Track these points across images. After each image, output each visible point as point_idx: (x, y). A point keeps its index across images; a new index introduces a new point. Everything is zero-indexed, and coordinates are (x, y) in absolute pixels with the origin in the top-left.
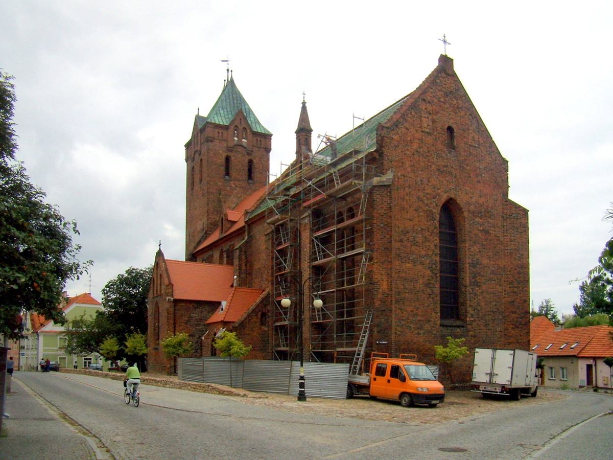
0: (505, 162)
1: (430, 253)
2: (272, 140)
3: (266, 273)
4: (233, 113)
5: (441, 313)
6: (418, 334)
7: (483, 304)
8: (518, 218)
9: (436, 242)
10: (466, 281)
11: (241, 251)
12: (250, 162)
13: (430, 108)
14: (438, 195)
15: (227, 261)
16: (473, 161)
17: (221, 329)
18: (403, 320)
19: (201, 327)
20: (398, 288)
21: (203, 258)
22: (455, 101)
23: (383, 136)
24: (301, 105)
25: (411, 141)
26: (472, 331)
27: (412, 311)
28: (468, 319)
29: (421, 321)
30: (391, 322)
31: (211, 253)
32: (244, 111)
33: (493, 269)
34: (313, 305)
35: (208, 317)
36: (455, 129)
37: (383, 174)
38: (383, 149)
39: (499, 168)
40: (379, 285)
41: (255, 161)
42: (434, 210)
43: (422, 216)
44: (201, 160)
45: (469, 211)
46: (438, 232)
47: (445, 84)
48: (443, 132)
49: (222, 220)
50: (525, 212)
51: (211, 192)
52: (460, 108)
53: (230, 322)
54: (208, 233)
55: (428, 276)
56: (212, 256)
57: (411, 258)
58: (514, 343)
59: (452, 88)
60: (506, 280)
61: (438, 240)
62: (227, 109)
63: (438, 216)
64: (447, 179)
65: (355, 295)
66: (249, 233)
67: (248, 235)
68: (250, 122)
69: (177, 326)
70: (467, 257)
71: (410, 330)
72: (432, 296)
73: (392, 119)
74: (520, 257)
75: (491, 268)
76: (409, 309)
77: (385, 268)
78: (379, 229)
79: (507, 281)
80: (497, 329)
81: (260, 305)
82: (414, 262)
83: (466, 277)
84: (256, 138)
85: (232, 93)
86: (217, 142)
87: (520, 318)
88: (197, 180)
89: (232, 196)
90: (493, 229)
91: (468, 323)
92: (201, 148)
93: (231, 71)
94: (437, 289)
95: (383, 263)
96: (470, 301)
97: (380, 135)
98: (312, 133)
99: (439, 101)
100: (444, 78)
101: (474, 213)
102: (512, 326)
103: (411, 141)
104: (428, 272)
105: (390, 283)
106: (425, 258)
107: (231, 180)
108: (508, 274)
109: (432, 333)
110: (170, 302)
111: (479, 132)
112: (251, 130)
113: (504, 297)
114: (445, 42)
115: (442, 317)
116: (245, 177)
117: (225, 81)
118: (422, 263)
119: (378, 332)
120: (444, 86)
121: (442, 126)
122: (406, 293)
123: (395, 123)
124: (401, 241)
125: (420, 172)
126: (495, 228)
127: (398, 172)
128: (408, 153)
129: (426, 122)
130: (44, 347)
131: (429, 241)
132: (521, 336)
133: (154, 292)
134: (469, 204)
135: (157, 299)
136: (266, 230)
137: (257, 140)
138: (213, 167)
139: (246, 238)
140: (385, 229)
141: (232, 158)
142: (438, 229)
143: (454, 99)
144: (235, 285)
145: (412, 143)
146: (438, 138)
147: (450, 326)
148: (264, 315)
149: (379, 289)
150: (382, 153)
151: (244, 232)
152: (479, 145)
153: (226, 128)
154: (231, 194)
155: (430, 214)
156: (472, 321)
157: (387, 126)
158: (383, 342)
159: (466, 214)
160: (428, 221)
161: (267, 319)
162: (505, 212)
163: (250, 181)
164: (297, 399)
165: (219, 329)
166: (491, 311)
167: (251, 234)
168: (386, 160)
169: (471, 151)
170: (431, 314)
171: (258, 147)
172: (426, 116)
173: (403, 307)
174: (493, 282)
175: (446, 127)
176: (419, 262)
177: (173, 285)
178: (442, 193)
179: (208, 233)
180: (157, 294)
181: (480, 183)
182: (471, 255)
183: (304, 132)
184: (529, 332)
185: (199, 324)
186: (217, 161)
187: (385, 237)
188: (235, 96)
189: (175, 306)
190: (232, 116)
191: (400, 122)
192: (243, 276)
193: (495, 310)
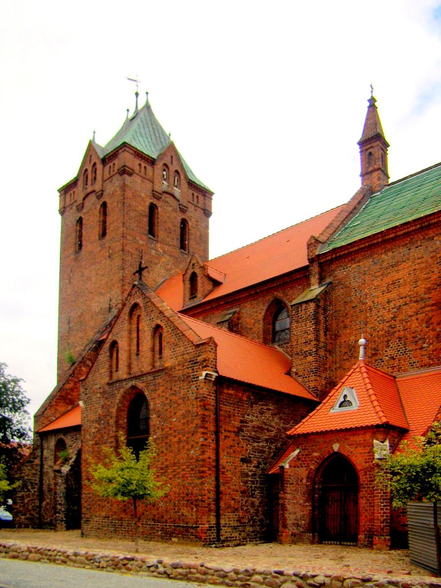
2: (213, 201)
12: (184, 222)
24: (368, 104)
51: (129, 251)
69: (222, 437)
86: (136, 179)
110: (210, 381)
112: (186, 177)
116: (177, 243)
138: (131, 214)
141: (159, 209)
154: (156, 261)
188: (155, 127)
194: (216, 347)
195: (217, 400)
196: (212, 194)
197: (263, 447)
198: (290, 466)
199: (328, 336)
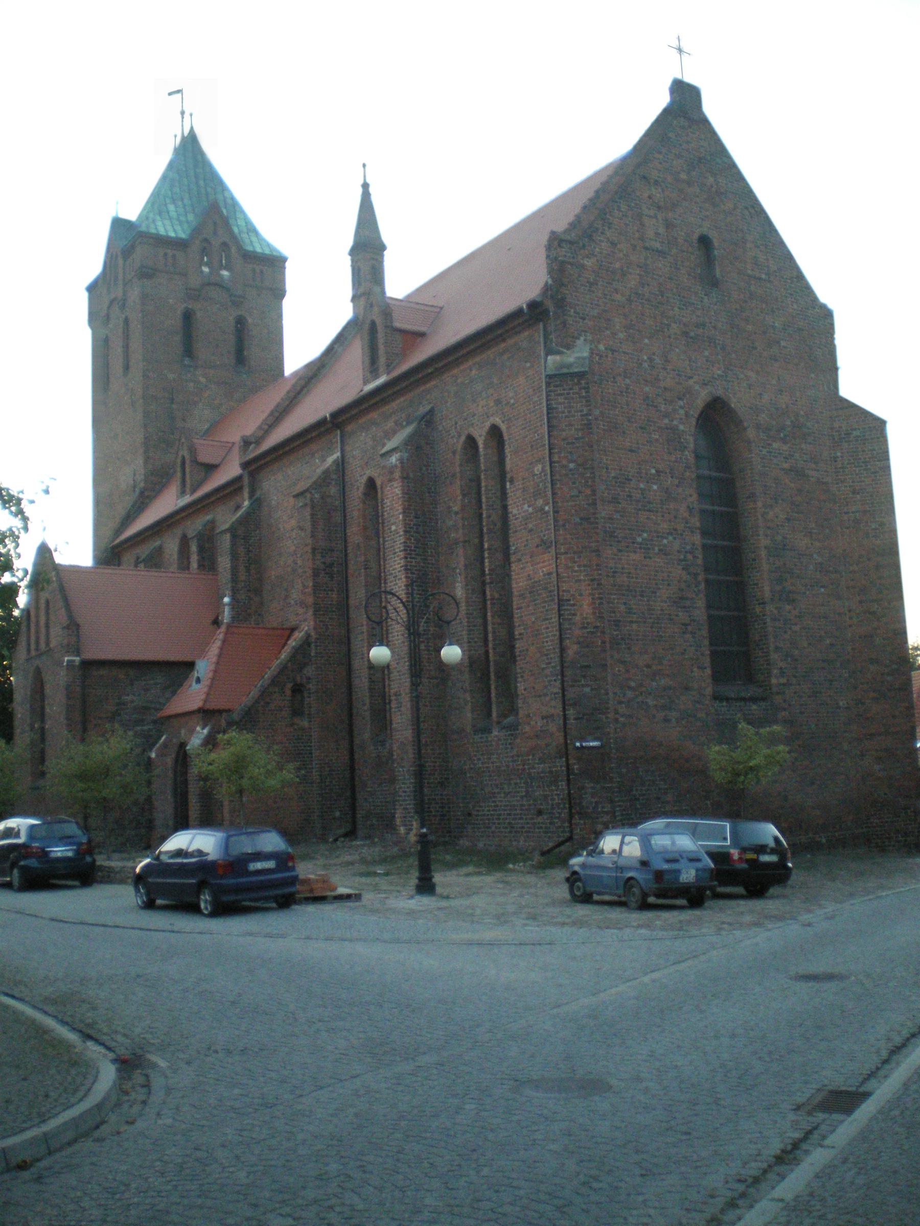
0: (826, 315)
1: (680, 527)
5: (713, 669)
7: (805, 644)
8: (865, 436)
9: (690, 500)
11: (234, 537)
15: (199, 561)
17: (198, 729)
19: (145, 728)
23: (563, 262)
24: (360, 191)
26: (785, 709)
27: (648, 666)
28: (774, 681)
30: (607, 694)
31: (158, 543)
32: (221, 204)
33: (820, 560)
34: (369, 660)
35: (162, 700)
37: (568, 349)
40: (574, 605)
41: (250, 321)
42: (681, 427)
43: (657, 440)
44: (126, 321)
46: (693, 476)
47: (688, 142)
49: (183, 463)
50: (882, 423)
52: (722, 193)
53: (220, 712)
54: (146, 494)
55: (679, 582)
61: (695, 496)
62: (182, 200)
63: (691, 439)
64: (706, 353)
65: (516, 633)
66: (252, 493)
67: (250, 498)
68: (236, 230)
70: (761, 533)
72: (690, 628)
75: (815, 556)
77: (585, 566)
78: (567, 475)
80: (841, 704)
81: (289, 665)
83: (763, 581)
87: (888, 674)
90: (814, 466)
91: (774, 690)
92: (125, 293)
93: (191, 115)
94: (700, 613)
97: (556, 259)
98: (385, 253)
100: (683, 127)
102: (872, 695)
103: (622, 270)
106: (671, 538)
108: (854, 572)
109: (695, 716)
111: (766, 246)
112: (240, 248)
114: (680, 50)
117: (176, 136)
118: (663, 552)
119: (575, 719)
122: (632, 622)
124: (615, 500)
126: (816, 463)
128: (618, 297)
132: (894, 717)
133: (29, 645)
135: (37, 662)
137: (166, 254)
139: (246, 503)
142: (693, 469)
144: (226, 615)
147: (737, 699)
148: (298, 689)
150: (563, 299)
151: (240, 489)
153: (180, 244)
156: (784, 684)
158: (591, 744)
159: (751, 433)
161: (307, 701)
162: (836, 425)
163: (187, 361)
164: (414, 892)
165: (192, 731)
166: (824, 661)
167: (258, 494)
169: (753, 288)
172: (652, 213)
175: (696, 236)
177: (78, 626)
178: (697, 387)
179: (146, 494)
180: (37, 649)
181: (776, 360)
182: (769, 528)
183: (368, 251)
185: (142, 720)
191: (597, 229)
192: (242, 596)
199: (253, 571)
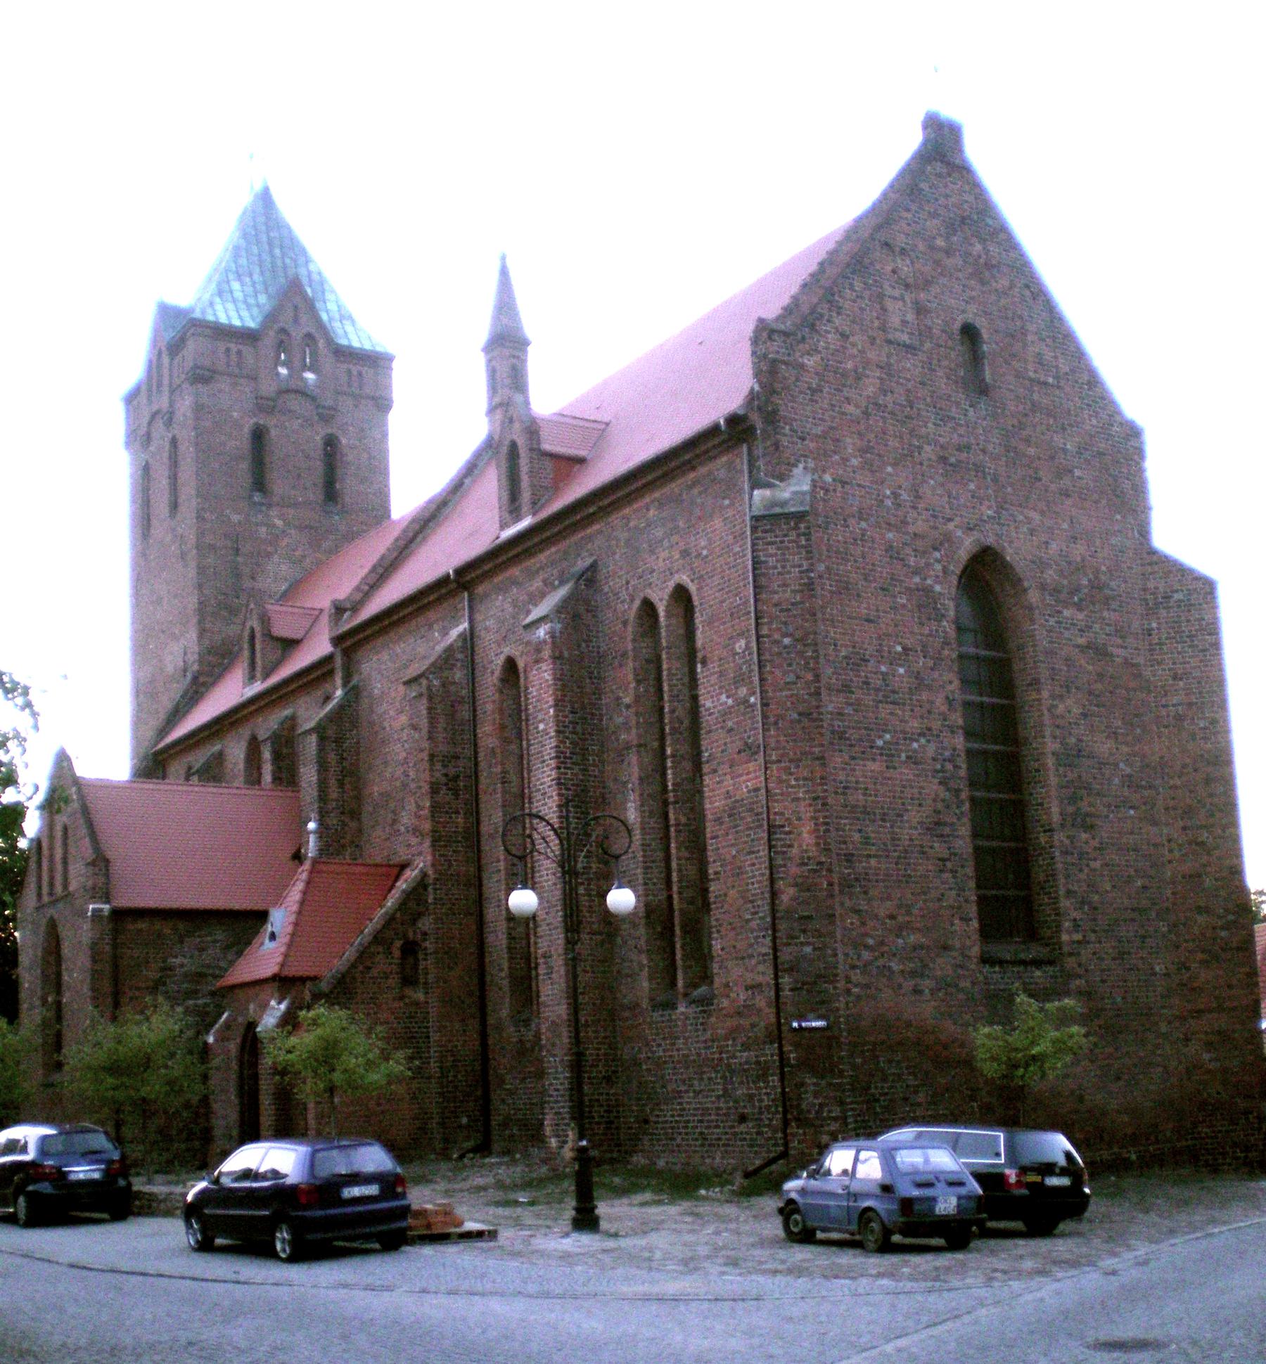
0: (1133, 433)
3: (413, 807)
4: (271, 290)
5: (981, 921)
6: (917, 991)
8: (1182, 608)
10: (1048, 814)
11: (322, 739)
13: (905, 268)
14: (948, 538)
15: (273, 773)
16: (1044, 427)
17: (273, 1003)
18: (866, 947)
20: (845, 843)
21: (190, 768)
22: (978, 247)
23: (774, 361)
25: (856, 371)
27: (892, 917)
28: (1065, 937)
29: (922, 947)
30: (835, 955)
31: (217, 748)
32: (305, 281)
33: (1128, 771)
35: (222, 964)
36: (985, 335)
37: (782, 480)
38: (775, 399)
39: (1113, 459)
41: (344, 441)
42: (938, 588)
43: (904, 606)
44: (174, 442)
45: (1043, 587)
47: (947, 196)
48: (950, 343)
49: (252, 637)
53: (303, 980)
54: (202, 679)
56: (220, 757)
57: (880, 743)
58: (1210, 1011)
59: (965, 206)
60: (1171, 803)
61: (956, 683)
62: (251, 275)
63: (951, 604)
64: (972, 486)
66: (347, 679)
68: (324, 317)
71: (889, 979)
72: (949, 865)
73: (797, 305)
74: (1205, 728)
75: (1122, 765)
76: (883, 910)
77: (805, 779)
79: (1174, 808)
80: (1157, 969)
81: (398, 915)
82: (888, 755)
83: (1050, 800)
84: (345, 366)
85: (266, 224)
86: (223, 384)
88: (161, 505)
89: (276, 558)
90: (1119, 641)
91: (1066, 949)
94: (963, 843)
95: (796, 761)
96: (1067, 877)
97: (765, 356)
99: (932, 248)
101: (1056, 591)
102: (1200, 956)
103: (856, 371)
104: (933, 787)
105: (822, 828)
106: (923, 741)
107: (270, 506)
111: (1054, 339)
112: (330, 341)
113: (1170, 862)
115: (986, 933)
116: (316, 495)
118: (913, 760)
120: (942, 201)
121: (946, 323)
122: (869, 856)
123: (804, 319)
124: (846, 688)
125: (889, 469)
127: (824, 471)
128: (851, 409)
129: (899, 312)
130: (1009, 659)
131: (930, 688)
132: (1230, 987)
133: (40, 887)
134: (1042, 565)
135: (51, 912)
136: (406, 667)
139: (339, 693)
140: (801, 654)
141: (273, 432)
143: (974, 240)
144: (312, 847)
145: (859, 379)
146: (935, 362)
147: (1014, 963)
148: (410, 949)
149: (790, 846)
150: (775, 412)
151: (331, 673)
152: (1057, 377)
153: (248, 336)
155: (926, 603)
156: (1079, 942)
157: (783, 327)
159: (1034, 596)
160: (922, 624)
161: (422, 965)
165: (264, 1006)
167: (354, 682)
168: (785, 435)
170: (952, 925)
171: (354, 396)
172: (896, 293)
173: (863, 906)
174: (1132, 812)
175: (957, 326)
176: (903, 756)
177: (107, 861)
179: (202, 679)
180: (51, 894)
184: (1256, 974)
186: (223, 444)
187: (798, 677)
189: (116, 932)
190: (270, 297)
191: (822, 316)
192: (333, 821)
193: (1145, 903)
194: (107, 867)
195: (115, 947)
196: (390, 359)
197: (206, 1005)
198: (216, 1040)
199: (348, 786)
